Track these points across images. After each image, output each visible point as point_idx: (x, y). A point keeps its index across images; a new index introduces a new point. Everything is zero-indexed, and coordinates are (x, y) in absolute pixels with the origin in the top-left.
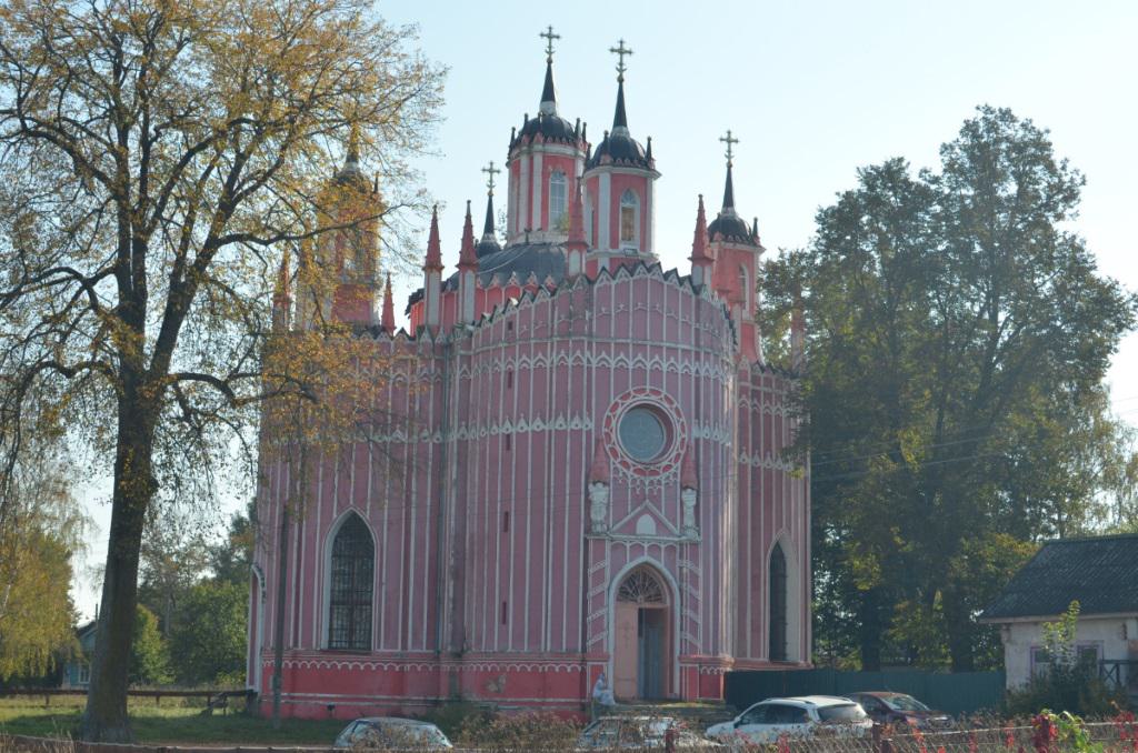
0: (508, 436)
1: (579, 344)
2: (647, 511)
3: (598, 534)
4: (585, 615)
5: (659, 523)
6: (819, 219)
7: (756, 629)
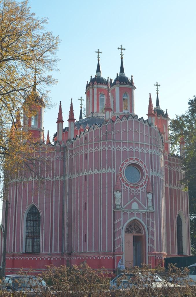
0: (86, 176)
1: (110, 143)
2: (135, 201)
3: (118, 209)
4: (114, 238)
5: (139, 205)
6: (189, 103)
7: (173, 244)
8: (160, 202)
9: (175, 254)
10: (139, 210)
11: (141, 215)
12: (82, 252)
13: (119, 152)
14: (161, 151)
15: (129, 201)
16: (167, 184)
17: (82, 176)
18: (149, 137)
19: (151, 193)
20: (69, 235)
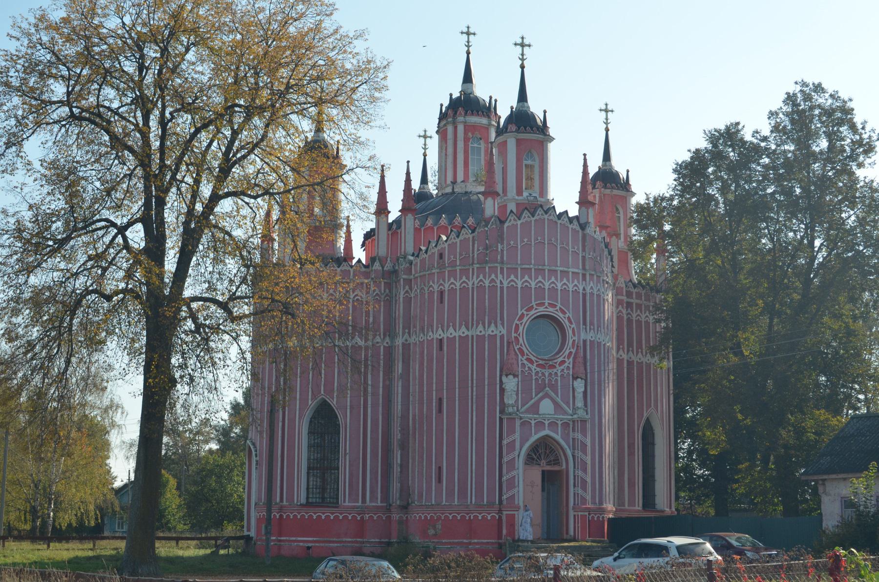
0: (441, 341)
1: (493, 270)
2: (547, 396)
3: (510, 414)
4: (501, 457)
6: (675, 171)
8: (603, 396)
9: (637, 508)
10: (556, 416)
11: (560, 425)
12: (432, 505)
13: (513, 289)
14: (607, 283)
15: (534, 396)
16: (621, 351)
17: (433, 339)
18: (581, 255)
19: (582, 379)
20: (404, 466)
